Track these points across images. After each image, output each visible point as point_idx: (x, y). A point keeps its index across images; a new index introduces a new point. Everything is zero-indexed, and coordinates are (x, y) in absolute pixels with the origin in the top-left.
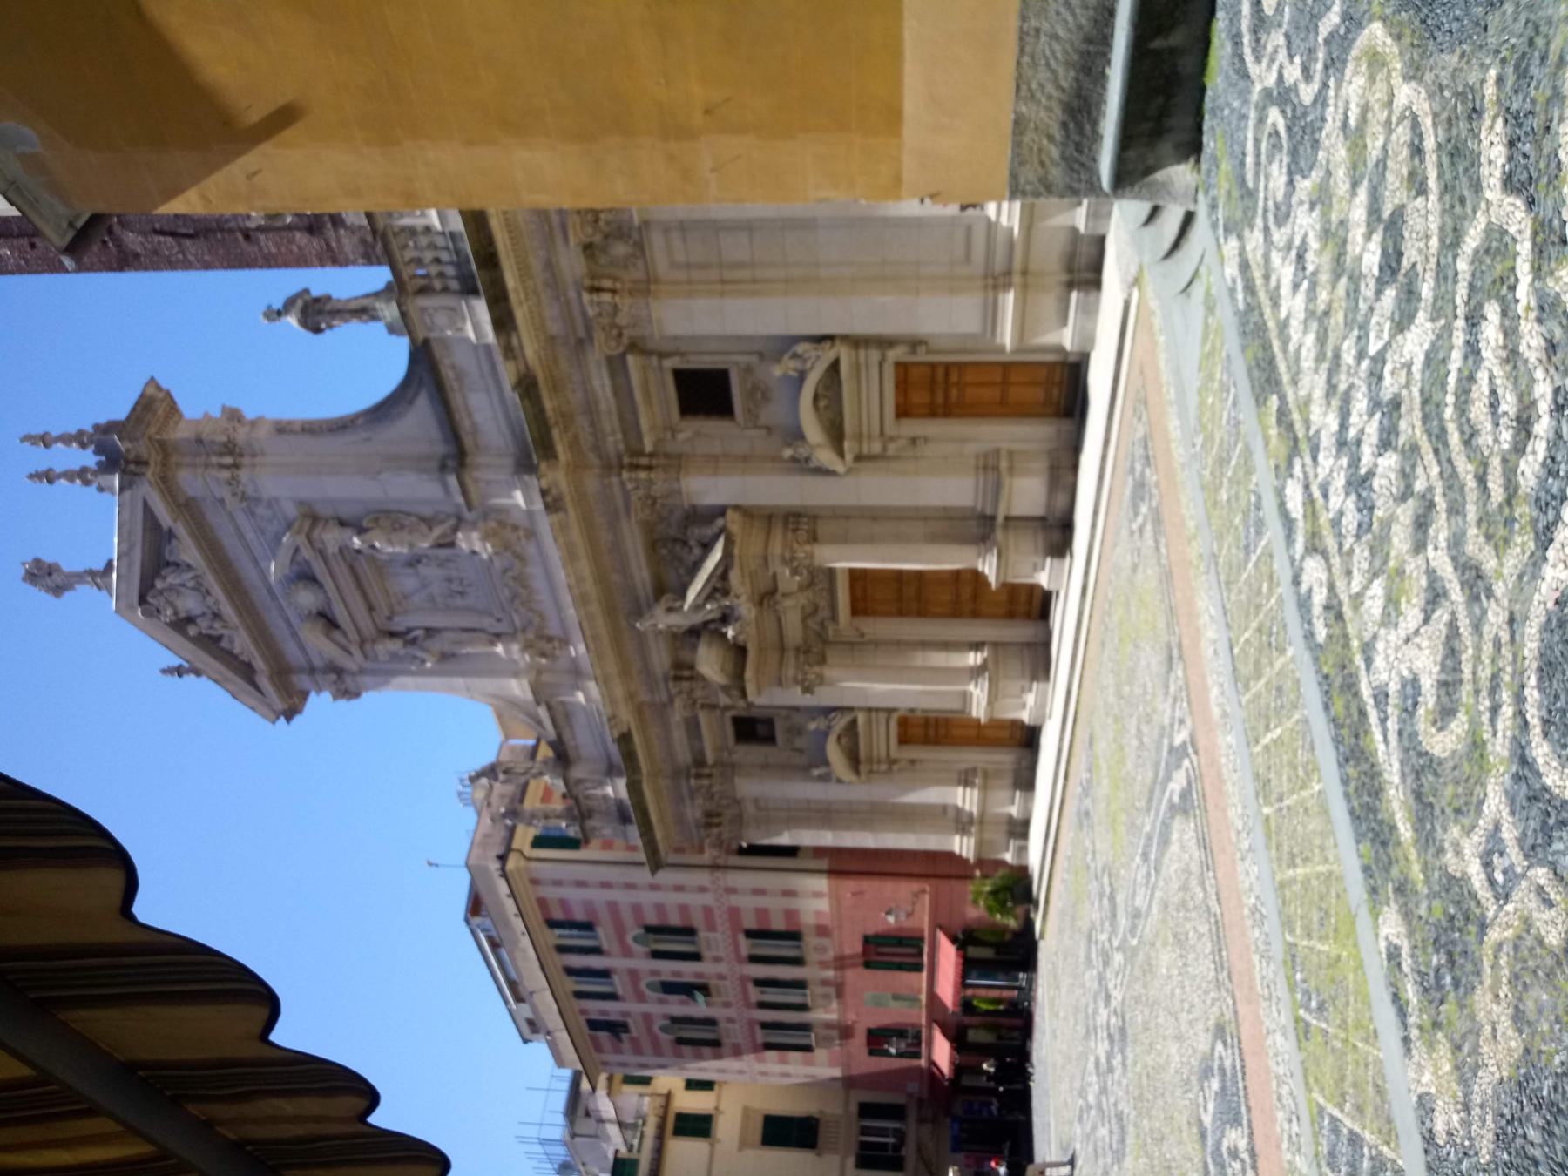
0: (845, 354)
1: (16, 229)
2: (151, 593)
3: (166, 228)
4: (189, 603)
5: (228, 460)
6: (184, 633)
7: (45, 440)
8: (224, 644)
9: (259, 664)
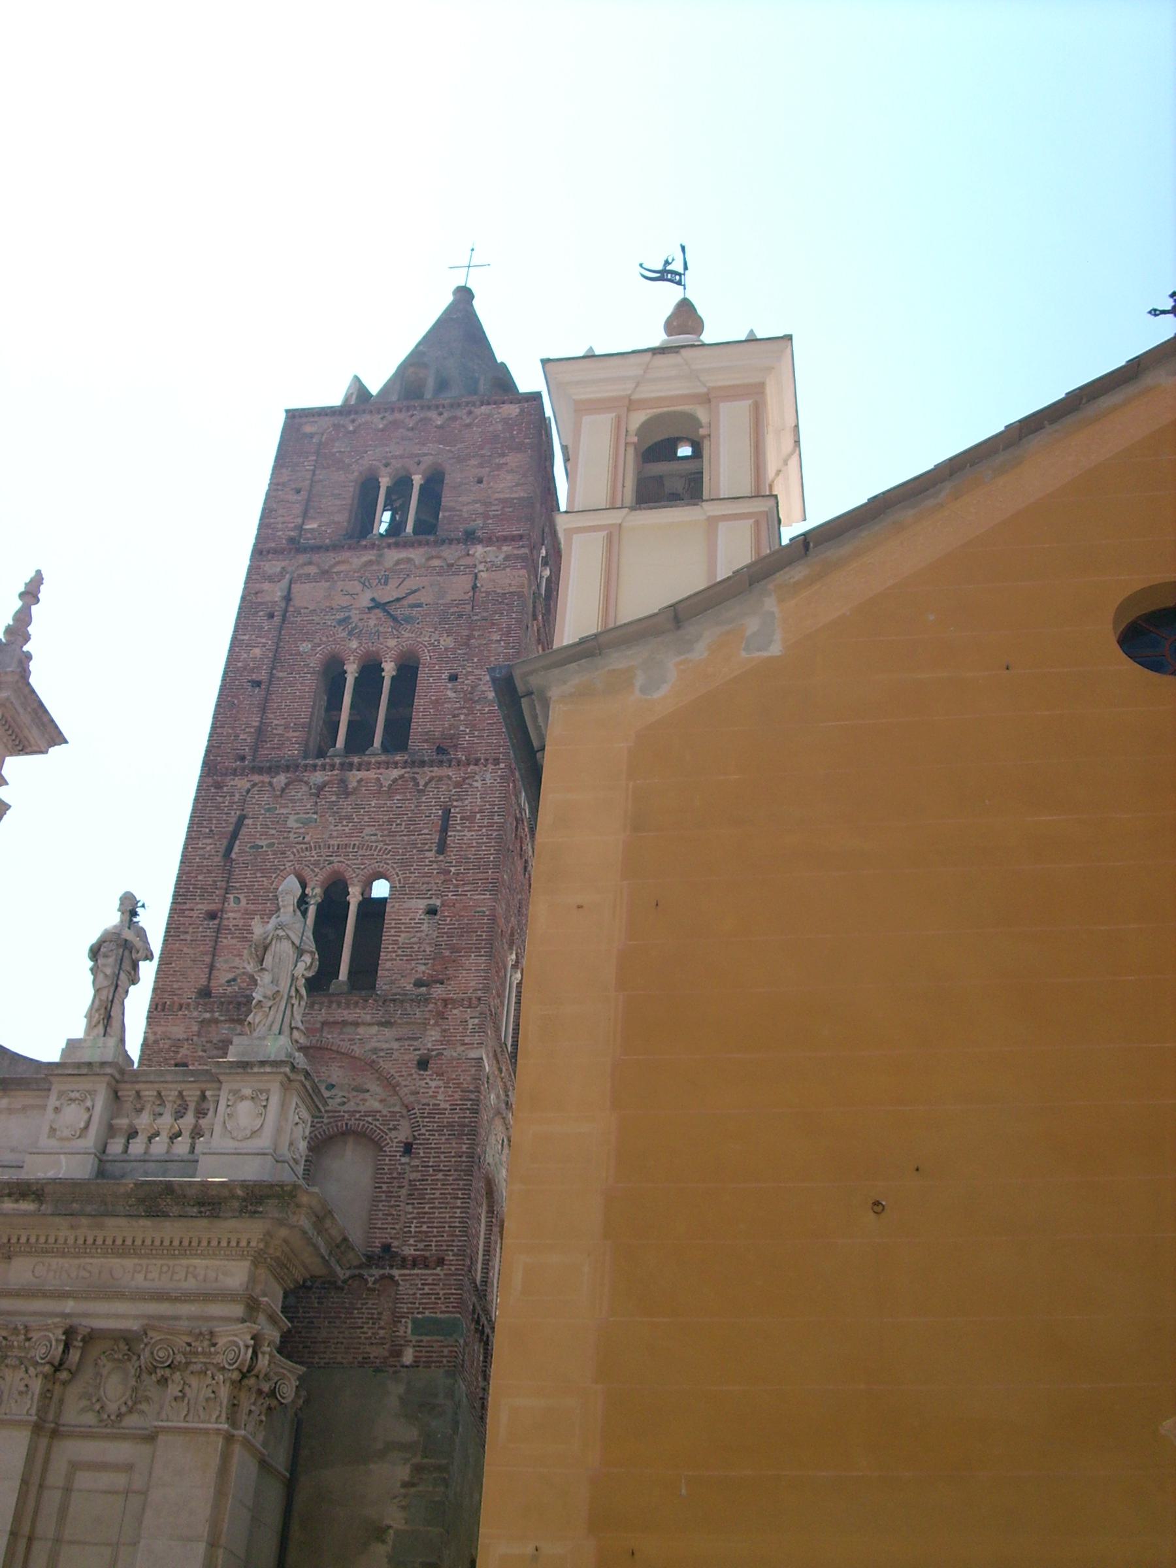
1: (281, 675)
3: (244, 830)
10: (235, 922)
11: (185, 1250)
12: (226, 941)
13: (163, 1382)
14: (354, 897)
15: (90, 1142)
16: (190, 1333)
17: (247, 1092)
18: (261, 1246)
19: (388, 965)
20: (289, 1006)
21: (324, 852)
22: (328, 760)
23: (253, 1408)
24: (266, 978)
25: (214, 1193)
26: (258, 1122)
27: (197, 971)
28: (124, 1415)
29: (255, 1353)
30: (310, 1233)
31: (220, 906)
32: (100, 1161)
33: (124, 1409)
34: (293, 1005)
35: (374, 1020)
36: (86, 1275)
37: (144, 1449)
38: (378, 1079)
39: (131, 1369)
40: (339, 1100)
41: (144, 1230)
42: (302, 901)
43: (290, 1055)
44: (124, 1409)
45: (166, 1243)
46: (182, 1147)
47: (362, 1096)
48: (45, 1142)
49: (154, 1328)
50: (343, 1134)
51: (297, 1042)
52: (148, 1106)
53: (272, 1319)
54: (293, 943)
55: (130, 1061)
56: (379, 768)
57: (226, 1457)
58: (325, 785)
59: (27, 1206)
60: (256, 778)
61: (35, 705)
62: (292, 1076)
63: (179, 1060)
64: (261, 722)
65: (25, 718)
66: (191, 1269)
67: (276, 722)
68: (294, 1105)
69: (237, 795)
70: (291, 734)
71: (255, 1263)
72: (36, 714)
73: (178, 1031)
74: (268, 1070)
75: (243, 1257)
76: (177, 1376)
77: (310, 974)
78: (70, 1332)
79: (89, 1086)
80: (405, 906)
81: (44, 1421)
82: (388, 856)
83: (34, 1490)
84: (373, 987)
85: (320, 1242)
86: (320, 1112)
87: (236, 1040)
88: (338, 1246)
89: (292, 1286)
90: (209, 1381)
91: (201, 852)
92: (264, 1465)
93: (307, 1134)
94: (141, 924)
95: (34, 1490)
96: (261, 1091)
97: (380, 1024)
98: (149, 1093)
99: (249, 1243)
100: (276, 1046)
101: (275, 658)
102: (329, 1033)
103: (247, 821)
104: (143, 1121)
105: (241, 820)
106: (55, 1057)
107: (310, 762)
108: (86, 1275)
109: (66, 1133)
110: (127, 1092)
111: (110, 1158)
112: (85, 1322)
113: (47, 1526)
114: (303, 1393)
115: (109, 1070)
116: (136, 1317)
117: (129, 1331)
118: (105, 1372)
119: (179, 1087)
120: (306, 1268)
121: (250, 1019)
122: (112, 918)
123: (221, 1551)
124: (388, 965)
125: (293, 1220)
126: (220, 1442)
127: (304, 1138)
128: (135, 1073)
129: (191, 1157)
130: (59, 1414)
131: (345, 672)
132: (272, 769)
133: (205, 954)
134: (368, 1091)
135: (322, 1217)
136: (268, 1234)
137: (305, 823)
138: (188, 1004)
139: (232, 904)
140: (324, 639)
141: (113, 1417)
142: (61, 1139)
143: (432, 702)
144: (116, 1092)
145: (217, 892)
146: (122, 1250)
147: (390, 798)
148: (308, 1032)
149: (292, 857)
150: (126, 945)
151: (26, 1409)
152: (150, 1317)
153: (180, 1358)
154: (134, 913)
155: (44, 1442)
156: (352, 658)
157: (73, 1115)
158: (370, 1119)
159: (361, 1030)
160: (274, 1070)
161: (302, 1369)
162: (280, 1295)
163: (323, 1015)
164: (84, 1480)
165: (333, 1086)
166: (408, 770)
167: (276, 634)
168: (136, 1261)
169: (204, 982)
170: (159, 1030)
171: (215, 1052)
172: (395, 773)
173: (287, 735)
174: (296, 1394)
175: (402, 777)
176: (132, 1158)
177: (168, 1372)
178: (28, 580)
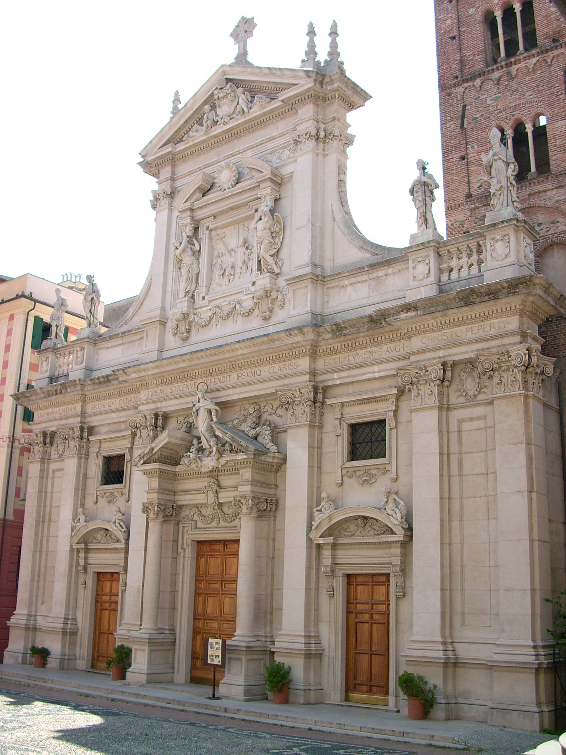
0: (399, 536)
1: (463, 29)
2: (234, 87)
3: (467, 112)
4: (224, 110)
5: (322, 135)
6: (205, 102)
7: (334, 33)
8: (196, 127)
9: (181, 147)
10: (474, 158)
11: (487, 317)
12: (473, 168)
13: (490, 377)
14: (529, 129)
15: (432, 278)
16: (498, 354)
17: (498, 237)
18: (522, 307)
19: (554, 157)
20: (509, 191)
21: (509, 111)
22: (498, 65)
23: (534, 381)
24: (494, 181)
25: (494, 288)
26: (507, 250)
27: (462, 186)
28: (477, 395)
29: (529, 356)
30: (544, 296)
31: (465, 152)
32: (439, 286)
33: (476, 393)
34: (511, 191)
35: (553, 187)
36: (445, 338)
37: (489, 408)
38: (562, 215)
39: (475, 374)
40: (545, 230)
41: (466, 312)
42: (503, 140)
43: (515, 215)
44: (476, 393)
45: (478, 316)
46: (474, 270)
47: (556, 225)
48: (413, 284)
49: (481, 355)
50: (551, 245)
51: (517, 207)
52: (455, 255)
53: (535, 339)
54: (503, 161)
55: (442, 238)
56: (525, 60)
57: (526, 405)
58: (500, 77)
59: (412, 314)
60: (466, 85)
61: (352, 85)
62: (518, 225)
63: (465, 231)
64: (461, 56)
65: (349, 93)
66: (492, 325)
67: (468, 54)
68: (522, 238)
69: (459, 96)
70: (477, 57)
71: (521, 316)
72: (354, 89)
73: (461, 217)
74: (506, 224)
75: (514, 314)
76: (415, 387)
77: (515, 173)
78: (444, 365)
79: (425, 254)
80: (556, 126)
81: (443, 405)
82: (541, 104)
83: (445, 434)
84: (549, 171)
85: (550, 299)
86: (536, 238)
87: (488, 214)
88: (559, 299)
89: (541, 322)
90: (511, 373)
91: (449, 129)
92: (546, 406)
93: (533, 250)
94: (429, 173)
95: (445, 434)
96: (505, 235)
97: (557, 188)
98: (453, 250)
99: (515, 307)
100: (507, 212)
101: (459, 22)
102: (533, 199)
103: (467, 108)
104: (454, 263)
105: (464, 107)
106: (408, 245)
107: (490, 68)
108: (445, 338)
109: (421, 277)
110: (443, 251)
111: (443, 283)
112: (450, 358)
113: (454, 448)
114: (558, 370)
115: (432, 244)
116: (473, 351)
117: (470, 358)
118: (464, 378)
119: (467, 243)
120: (547, 313)
121: (492, 203)
122: (416, 174)
123: (533, 446)
124: (554, 157)
125: (534, 292)
126: (522, 399)
127: (532, 252)
128: (445, 242)
129: (480, 274)
130: (448, 400)
131: (495, 17)
132: (473, 78)
133: (463, 177)
134: (558, 222)
135: (547, 288)
136: (524, 301)
137: (496, 100)
138: (463, 203)
139: (471, 150)
140: (481, 3)
141: (472, 397)
142: (419, 280)
143: (544, 17)
144: (438, 253)
145: (462, 146)
146: (459, 323)
147: (535, 74)
148: (522, 202)
149: (494, 119)
150: (425, 184)
151: (433, 401)
152: (479, 350)
153: (495, 365)
154: (424, 169)
155: (444, 413)
156: (497, 8)
157: (422, 269)
158: (562, 235)
159: (548, 193)
160: (509, 224)
161: (554, 359)
162: (537, 328)
163: (528, 191)
164: (466, 426)
165: (541, 224)
166: (540, 56)
167: (456, 9)
168: (466, 327)
169: (467, 191)
170: (452, 219)
171: (481, 222)
172: (534, 60)
173: (475, 59)
174: (554, 371)
175: (538, 61)
176: (453, 281)
177: (492, 373)
178: (235, 56)
